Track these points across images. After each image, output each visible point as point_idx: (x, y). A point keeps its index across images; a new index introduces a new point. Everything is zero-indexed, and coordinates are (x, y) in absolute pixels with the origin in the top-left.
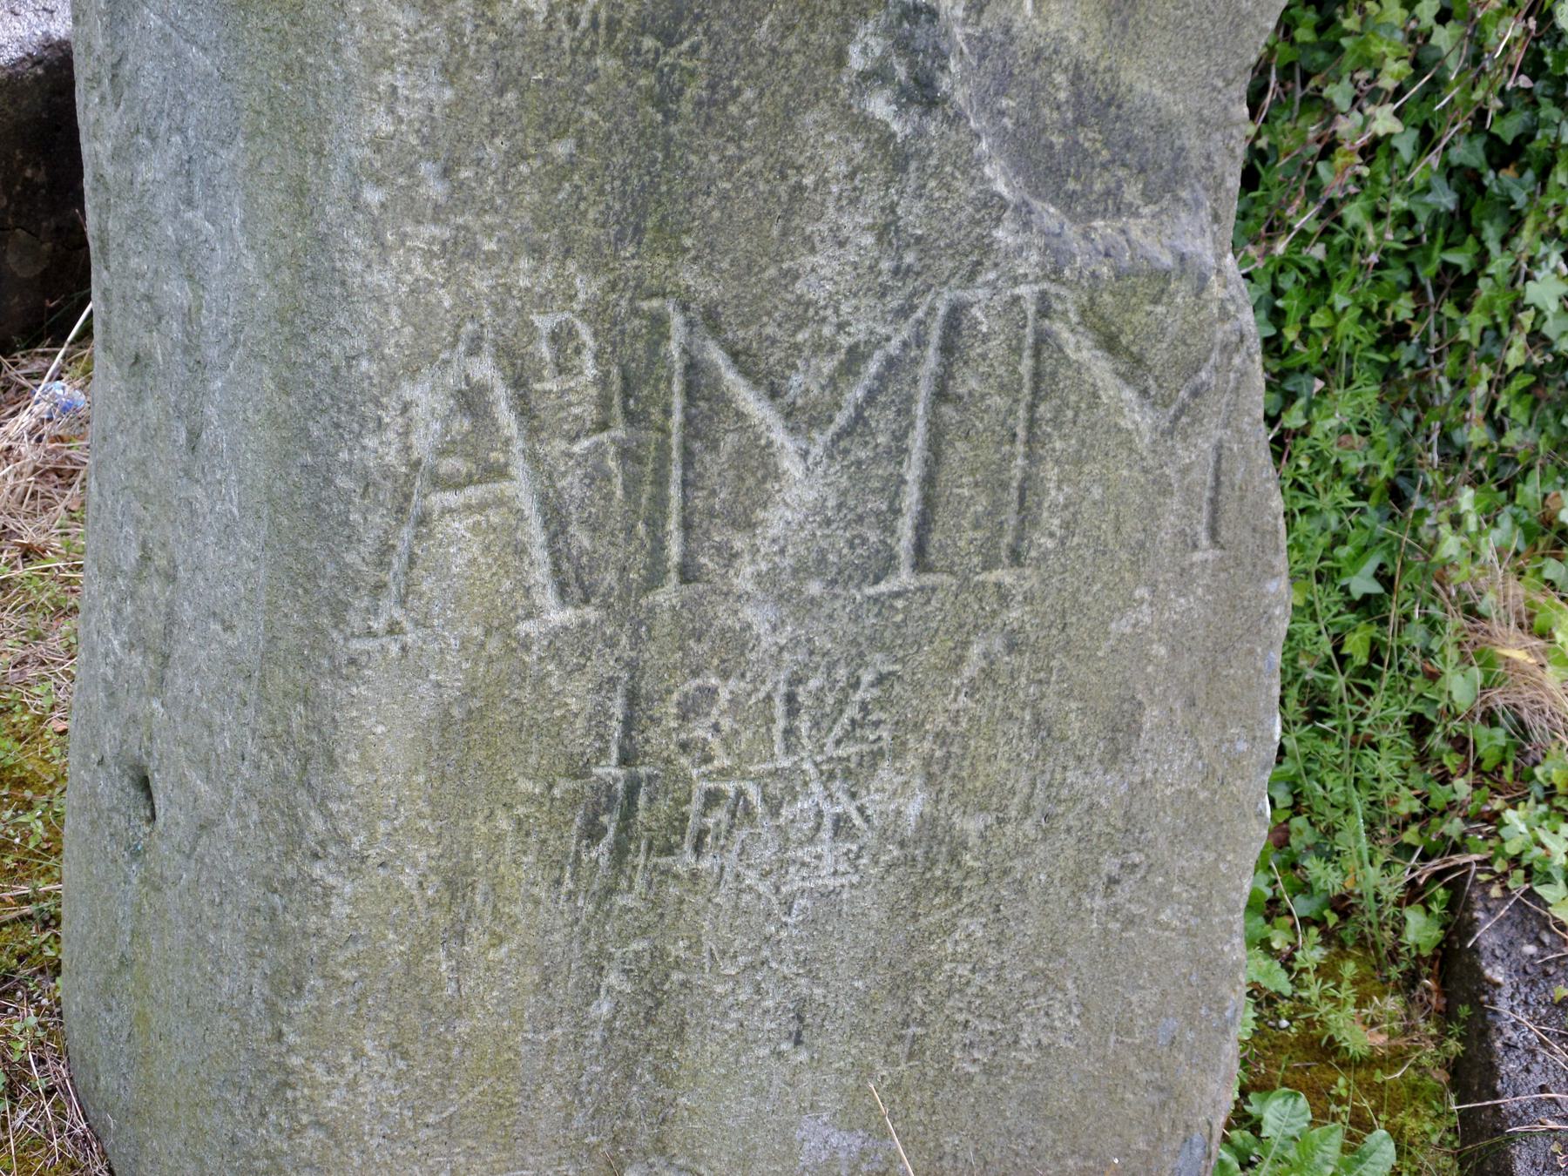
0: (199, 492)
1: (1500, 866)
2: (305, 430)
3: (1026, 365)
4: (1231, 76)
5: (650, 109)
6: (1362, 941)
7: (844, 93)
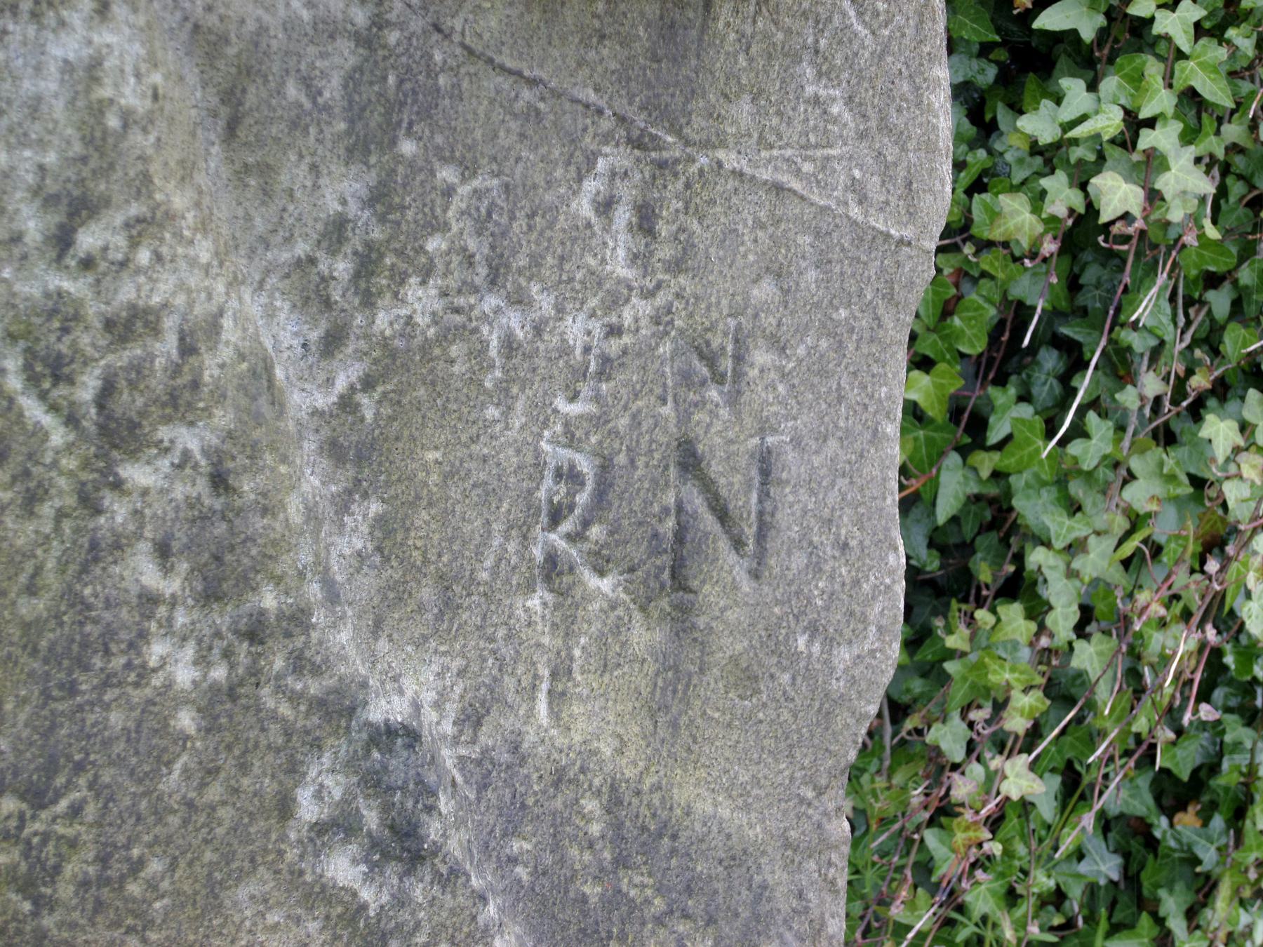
4: (823, 782)
5: (13, 897)
7: (291, 855)
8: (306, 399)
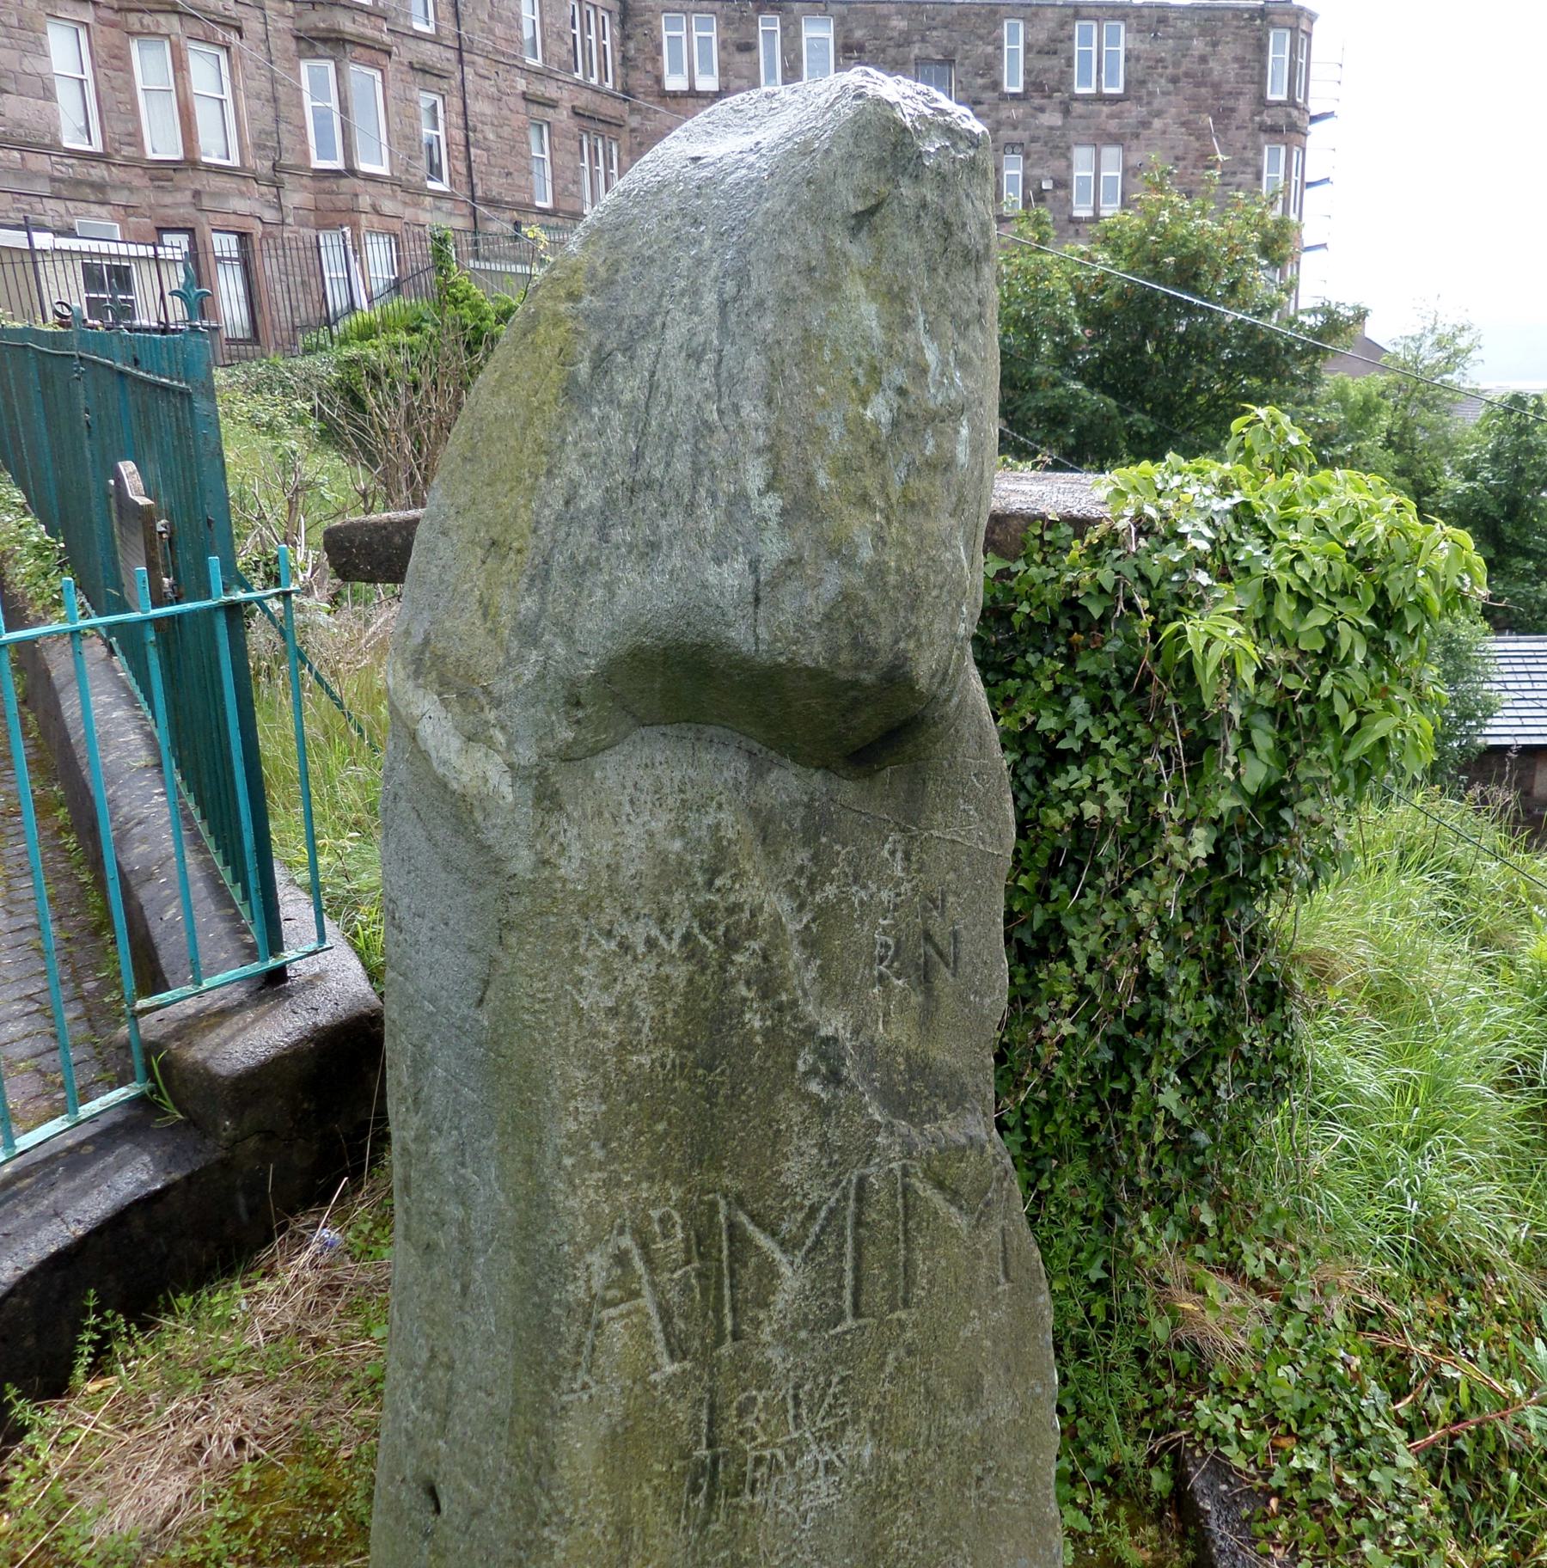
0: (468, 1319)
1: (1198, 1437)
2: (535, 1286)
3: (900, 1203)
6: (1128, 1493)
8: (793, 927)
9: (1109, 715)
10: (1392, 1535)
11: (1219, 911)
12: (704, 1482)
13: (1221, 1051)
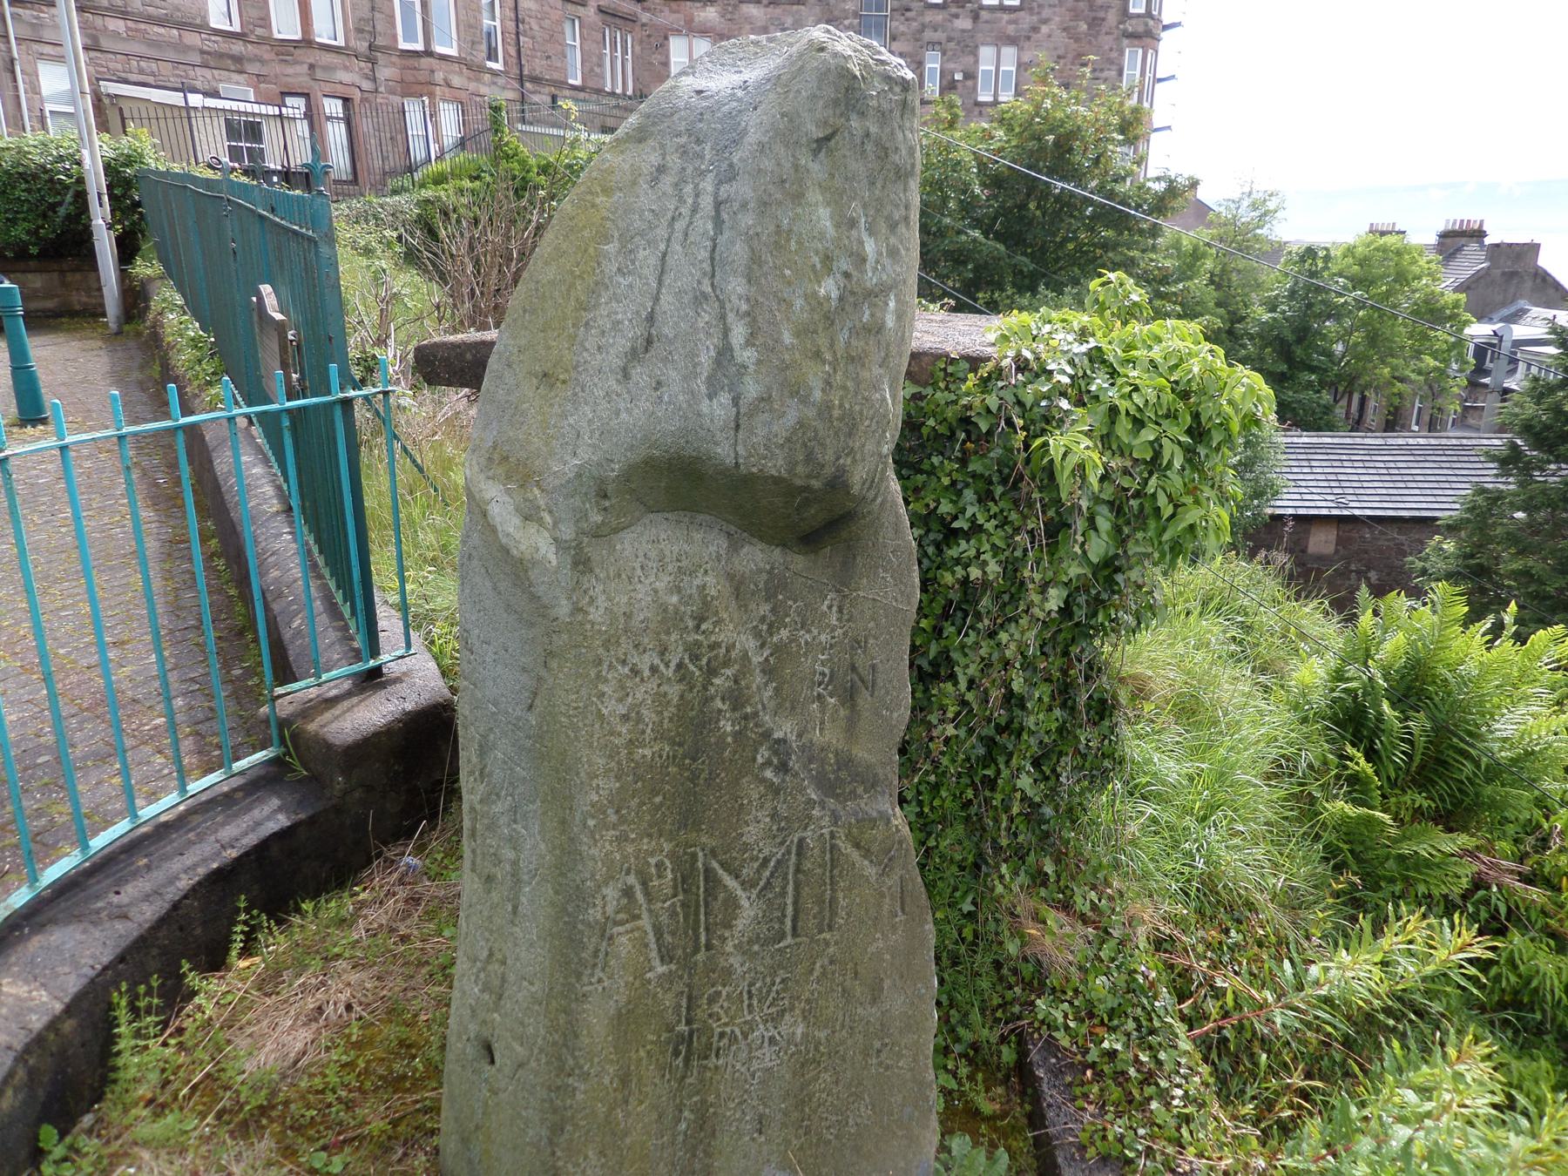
1: (1036, 1025)
3: (828, 856)
6: (985, 1063)
8: (757, 659)
9: (991, 504)
10: (1173, 1098)
11: (1067, 646)
12: (683, 1049)
13: (1065, 749)
